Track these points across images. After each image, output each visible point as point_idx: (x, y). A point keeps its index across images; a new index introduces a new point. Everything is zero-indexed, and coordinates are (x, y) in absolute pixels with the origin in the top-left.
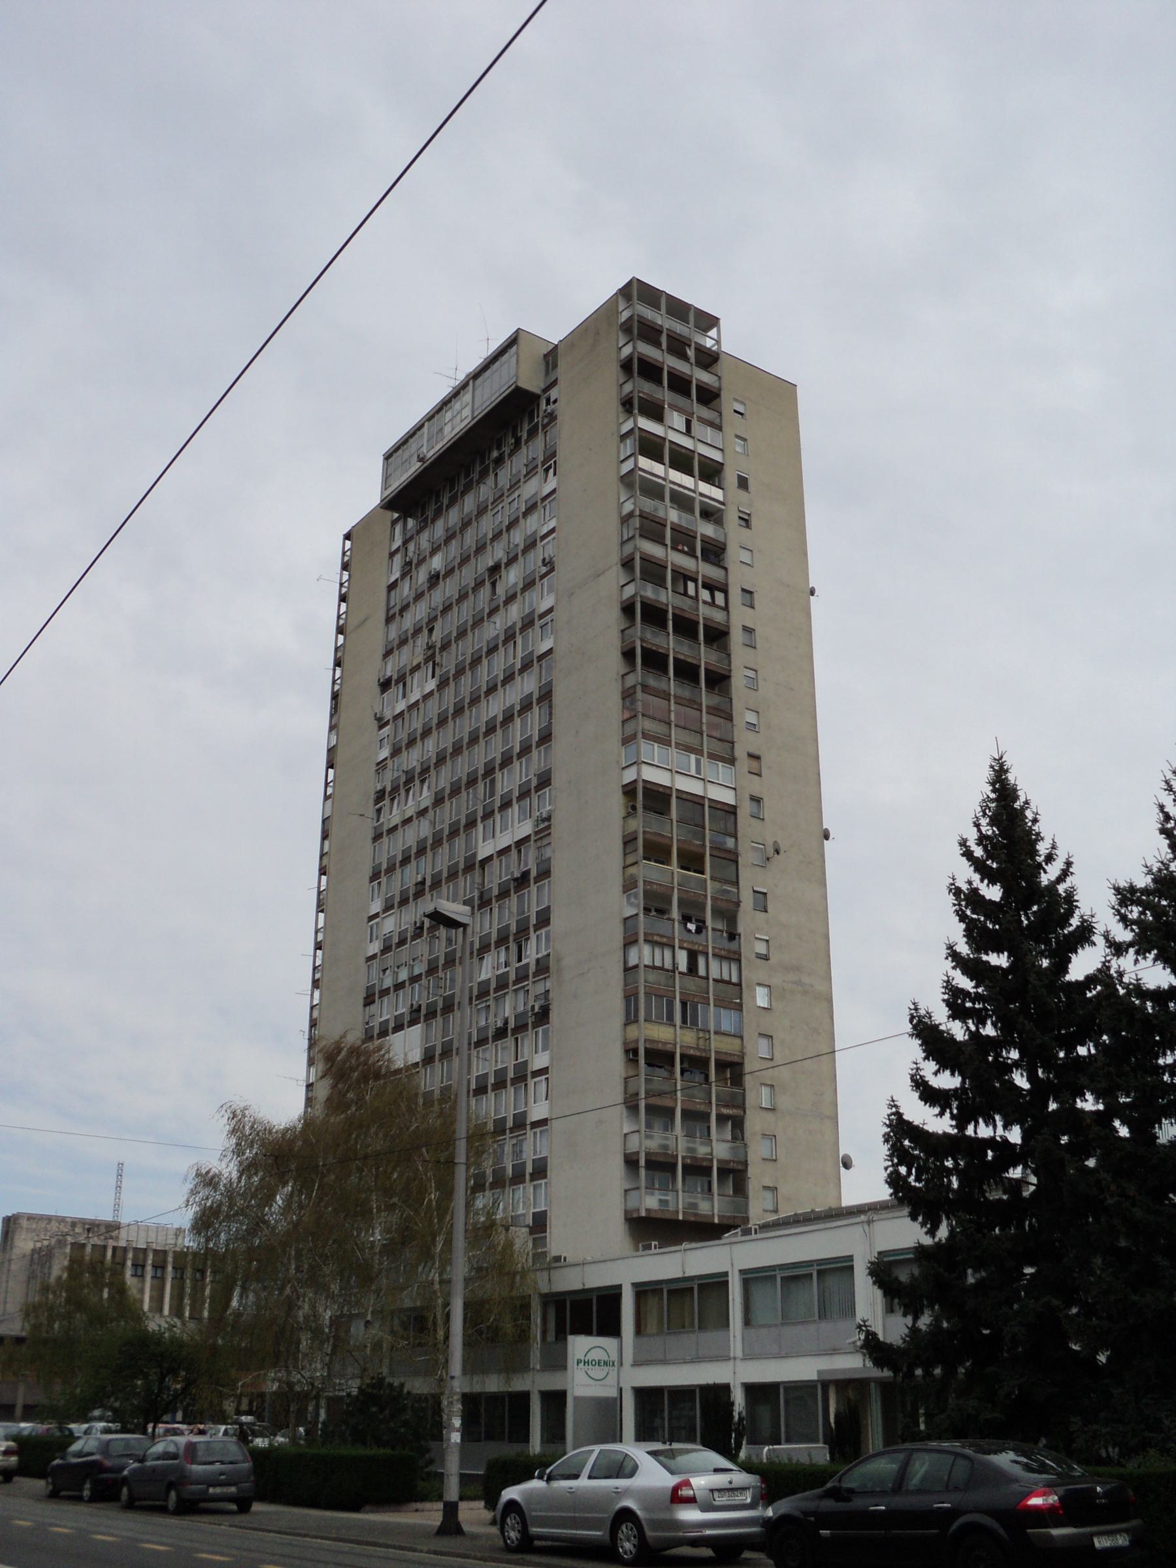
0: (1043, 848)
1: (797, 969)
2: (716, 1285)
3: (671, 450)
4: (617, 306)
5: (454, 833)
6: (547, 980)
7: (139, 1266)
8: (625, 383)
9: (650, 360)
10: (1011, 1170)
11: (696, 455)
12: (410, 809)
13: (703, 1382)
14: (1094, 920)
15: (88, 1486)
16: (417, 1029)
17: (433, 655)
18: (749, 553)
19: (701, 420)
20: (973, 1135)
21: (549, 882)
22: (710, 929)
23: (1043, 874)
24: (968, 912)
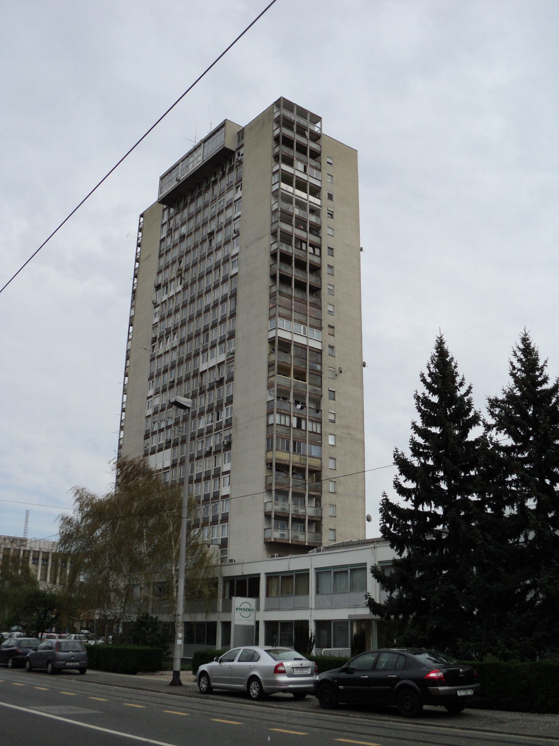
0: (458, 380)
1: (348, 427)
2: (303, 575)
3: (296, 180)
4: (273, 111)
5: (189, 359)
6: (231, 430)
7: (36, 560)
8: (275, 147)
9: (288, 137)
10: (438, 527)
11: (308, 183)
12: (168, 347)
13: (296, 619)
14: (480, 414)
15: (11, 661)
16: (169, 450)
17: (181, 274)
18: (332, 230)
19: (311, 166)
20: (421, 510)
21: (233, 383)
22: (308, 407)
23: (458, 392)
24: (423, 408)
